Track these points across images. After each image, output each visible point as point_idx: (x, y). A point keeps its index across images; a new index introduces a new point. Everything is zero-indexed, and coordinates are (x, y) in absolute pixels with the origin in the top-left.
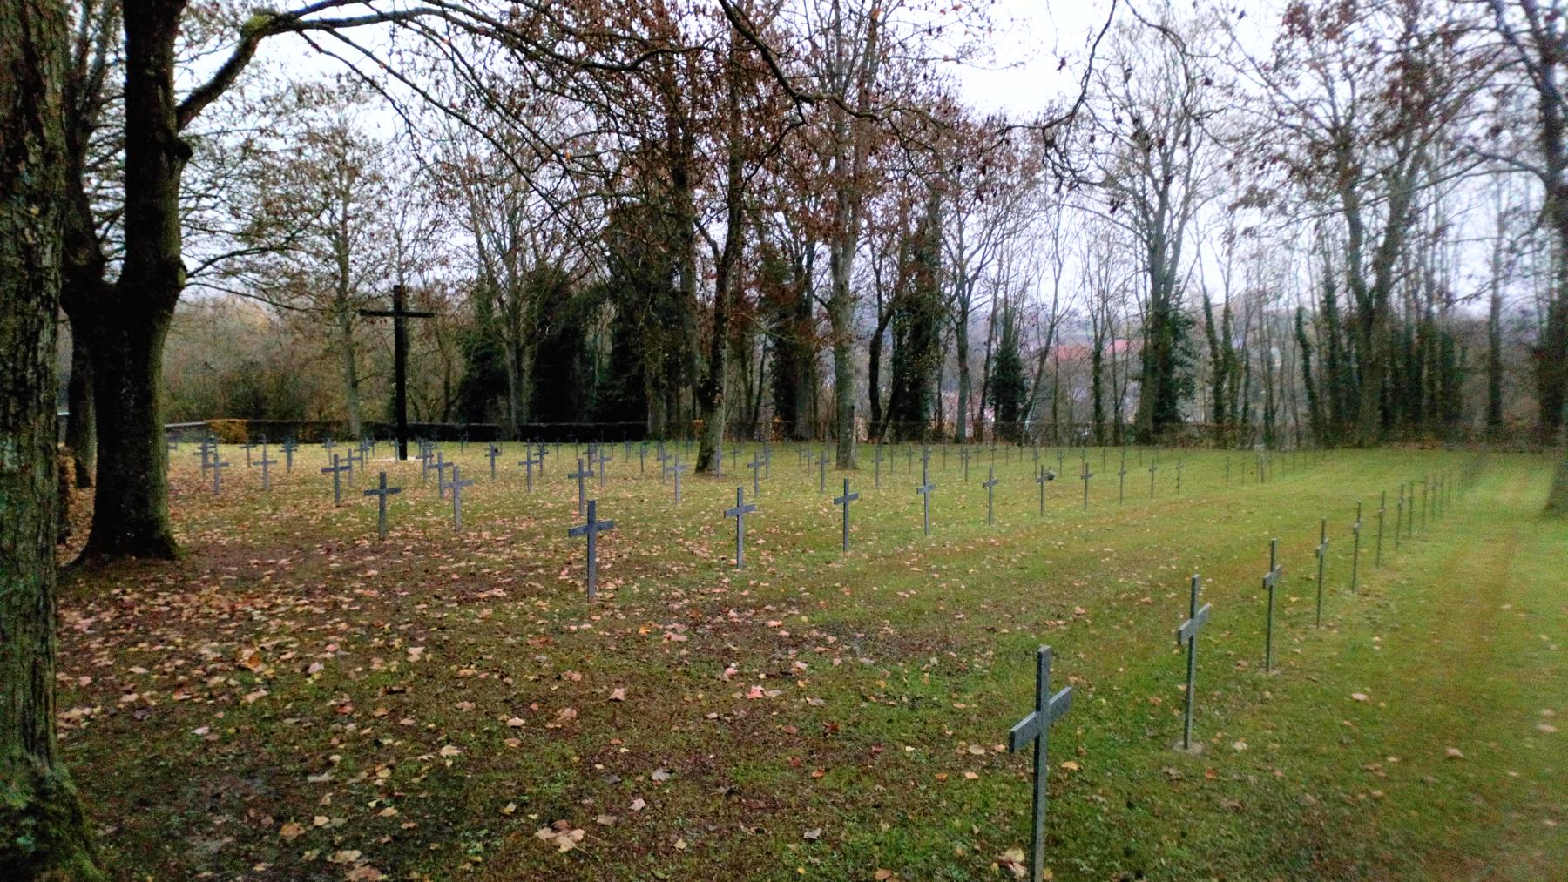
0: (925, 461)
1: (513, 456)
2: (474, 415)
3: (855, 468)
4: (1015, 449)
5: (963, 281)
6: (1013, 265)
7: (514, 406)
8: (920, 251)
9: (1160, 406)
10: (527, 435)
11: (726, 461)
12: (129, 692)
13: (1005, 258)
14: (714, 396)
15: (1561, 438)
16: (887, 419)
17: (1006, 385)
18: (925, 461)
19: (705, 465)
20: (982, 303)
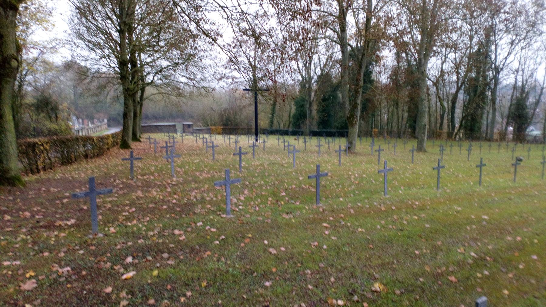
0: (469, 150)
1: (313, 142)
2: (296, 127)
3: (425, 151)
4: (350, 154)
5: (497, 70)
6: (527, 62)
7: (306, 126)
8: (480, 60)
9: (415, 122)
10: (315, 134)
11: (427, 144)
12: (489, 178)
13: (523, 59)
14: (353, 120)
15: (50, 5)
16: (459, 130)
17: (520, 115)
18: (469, 150)
19: (350, 149)
20: (507, 79)
